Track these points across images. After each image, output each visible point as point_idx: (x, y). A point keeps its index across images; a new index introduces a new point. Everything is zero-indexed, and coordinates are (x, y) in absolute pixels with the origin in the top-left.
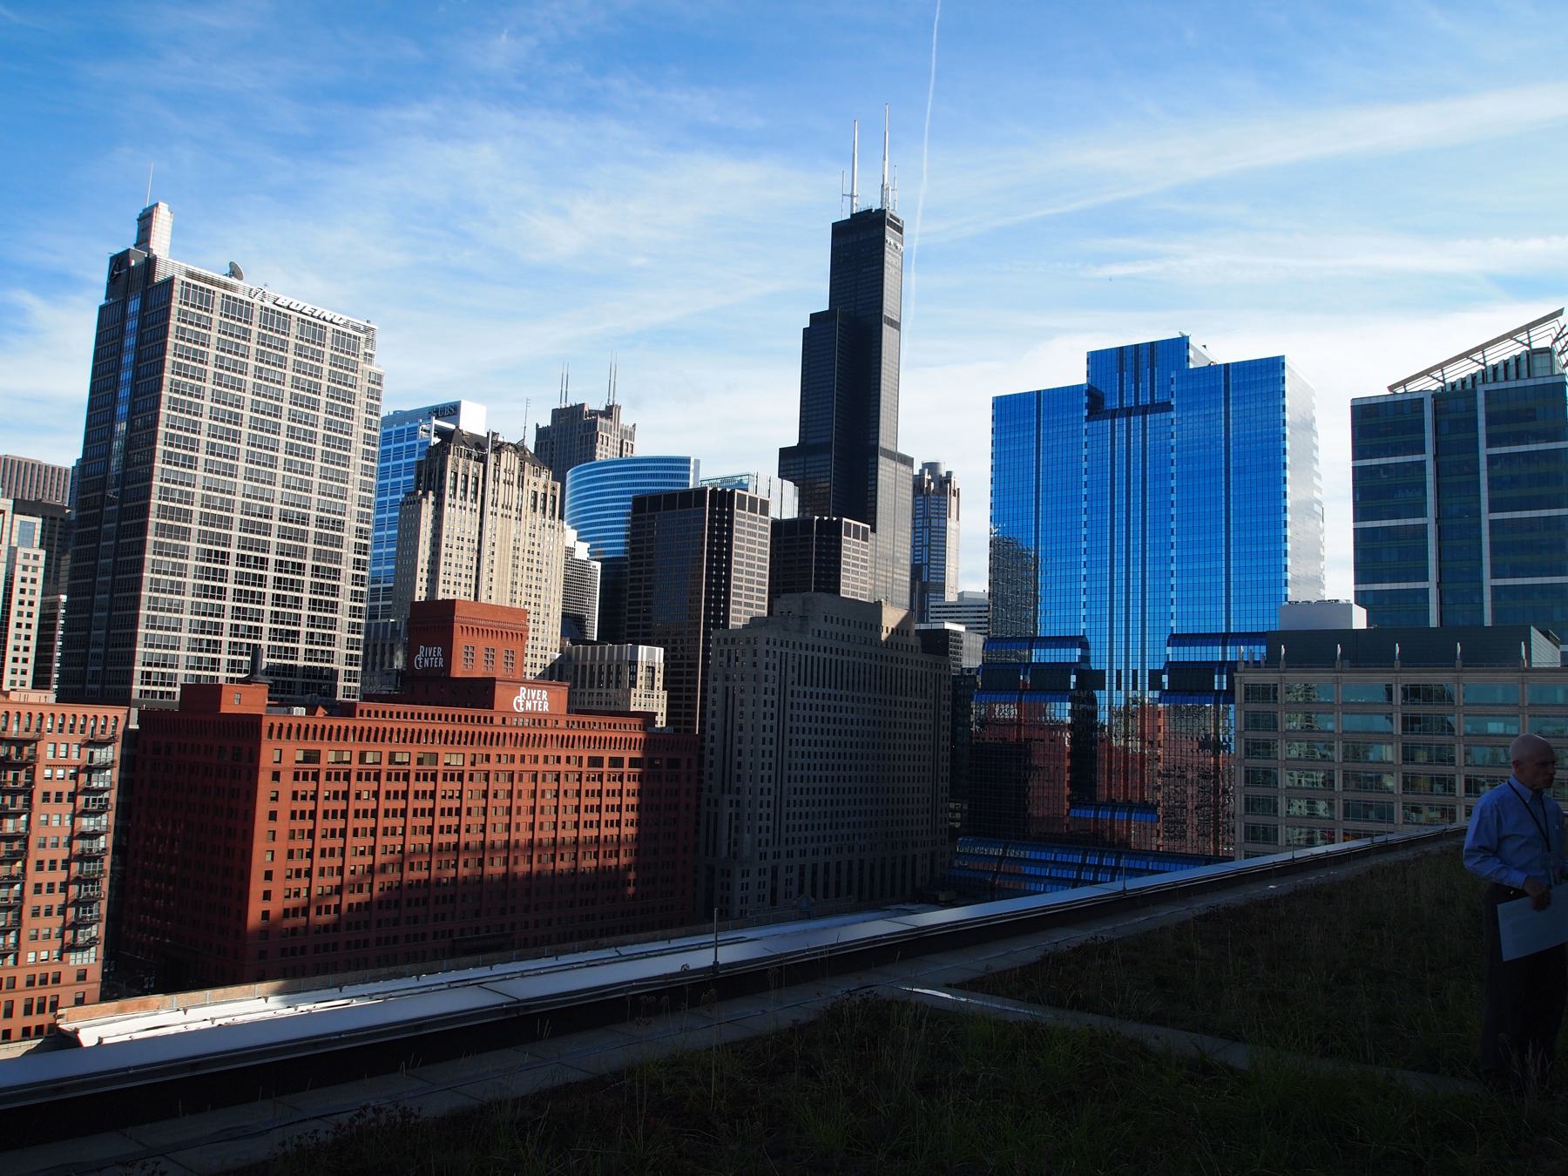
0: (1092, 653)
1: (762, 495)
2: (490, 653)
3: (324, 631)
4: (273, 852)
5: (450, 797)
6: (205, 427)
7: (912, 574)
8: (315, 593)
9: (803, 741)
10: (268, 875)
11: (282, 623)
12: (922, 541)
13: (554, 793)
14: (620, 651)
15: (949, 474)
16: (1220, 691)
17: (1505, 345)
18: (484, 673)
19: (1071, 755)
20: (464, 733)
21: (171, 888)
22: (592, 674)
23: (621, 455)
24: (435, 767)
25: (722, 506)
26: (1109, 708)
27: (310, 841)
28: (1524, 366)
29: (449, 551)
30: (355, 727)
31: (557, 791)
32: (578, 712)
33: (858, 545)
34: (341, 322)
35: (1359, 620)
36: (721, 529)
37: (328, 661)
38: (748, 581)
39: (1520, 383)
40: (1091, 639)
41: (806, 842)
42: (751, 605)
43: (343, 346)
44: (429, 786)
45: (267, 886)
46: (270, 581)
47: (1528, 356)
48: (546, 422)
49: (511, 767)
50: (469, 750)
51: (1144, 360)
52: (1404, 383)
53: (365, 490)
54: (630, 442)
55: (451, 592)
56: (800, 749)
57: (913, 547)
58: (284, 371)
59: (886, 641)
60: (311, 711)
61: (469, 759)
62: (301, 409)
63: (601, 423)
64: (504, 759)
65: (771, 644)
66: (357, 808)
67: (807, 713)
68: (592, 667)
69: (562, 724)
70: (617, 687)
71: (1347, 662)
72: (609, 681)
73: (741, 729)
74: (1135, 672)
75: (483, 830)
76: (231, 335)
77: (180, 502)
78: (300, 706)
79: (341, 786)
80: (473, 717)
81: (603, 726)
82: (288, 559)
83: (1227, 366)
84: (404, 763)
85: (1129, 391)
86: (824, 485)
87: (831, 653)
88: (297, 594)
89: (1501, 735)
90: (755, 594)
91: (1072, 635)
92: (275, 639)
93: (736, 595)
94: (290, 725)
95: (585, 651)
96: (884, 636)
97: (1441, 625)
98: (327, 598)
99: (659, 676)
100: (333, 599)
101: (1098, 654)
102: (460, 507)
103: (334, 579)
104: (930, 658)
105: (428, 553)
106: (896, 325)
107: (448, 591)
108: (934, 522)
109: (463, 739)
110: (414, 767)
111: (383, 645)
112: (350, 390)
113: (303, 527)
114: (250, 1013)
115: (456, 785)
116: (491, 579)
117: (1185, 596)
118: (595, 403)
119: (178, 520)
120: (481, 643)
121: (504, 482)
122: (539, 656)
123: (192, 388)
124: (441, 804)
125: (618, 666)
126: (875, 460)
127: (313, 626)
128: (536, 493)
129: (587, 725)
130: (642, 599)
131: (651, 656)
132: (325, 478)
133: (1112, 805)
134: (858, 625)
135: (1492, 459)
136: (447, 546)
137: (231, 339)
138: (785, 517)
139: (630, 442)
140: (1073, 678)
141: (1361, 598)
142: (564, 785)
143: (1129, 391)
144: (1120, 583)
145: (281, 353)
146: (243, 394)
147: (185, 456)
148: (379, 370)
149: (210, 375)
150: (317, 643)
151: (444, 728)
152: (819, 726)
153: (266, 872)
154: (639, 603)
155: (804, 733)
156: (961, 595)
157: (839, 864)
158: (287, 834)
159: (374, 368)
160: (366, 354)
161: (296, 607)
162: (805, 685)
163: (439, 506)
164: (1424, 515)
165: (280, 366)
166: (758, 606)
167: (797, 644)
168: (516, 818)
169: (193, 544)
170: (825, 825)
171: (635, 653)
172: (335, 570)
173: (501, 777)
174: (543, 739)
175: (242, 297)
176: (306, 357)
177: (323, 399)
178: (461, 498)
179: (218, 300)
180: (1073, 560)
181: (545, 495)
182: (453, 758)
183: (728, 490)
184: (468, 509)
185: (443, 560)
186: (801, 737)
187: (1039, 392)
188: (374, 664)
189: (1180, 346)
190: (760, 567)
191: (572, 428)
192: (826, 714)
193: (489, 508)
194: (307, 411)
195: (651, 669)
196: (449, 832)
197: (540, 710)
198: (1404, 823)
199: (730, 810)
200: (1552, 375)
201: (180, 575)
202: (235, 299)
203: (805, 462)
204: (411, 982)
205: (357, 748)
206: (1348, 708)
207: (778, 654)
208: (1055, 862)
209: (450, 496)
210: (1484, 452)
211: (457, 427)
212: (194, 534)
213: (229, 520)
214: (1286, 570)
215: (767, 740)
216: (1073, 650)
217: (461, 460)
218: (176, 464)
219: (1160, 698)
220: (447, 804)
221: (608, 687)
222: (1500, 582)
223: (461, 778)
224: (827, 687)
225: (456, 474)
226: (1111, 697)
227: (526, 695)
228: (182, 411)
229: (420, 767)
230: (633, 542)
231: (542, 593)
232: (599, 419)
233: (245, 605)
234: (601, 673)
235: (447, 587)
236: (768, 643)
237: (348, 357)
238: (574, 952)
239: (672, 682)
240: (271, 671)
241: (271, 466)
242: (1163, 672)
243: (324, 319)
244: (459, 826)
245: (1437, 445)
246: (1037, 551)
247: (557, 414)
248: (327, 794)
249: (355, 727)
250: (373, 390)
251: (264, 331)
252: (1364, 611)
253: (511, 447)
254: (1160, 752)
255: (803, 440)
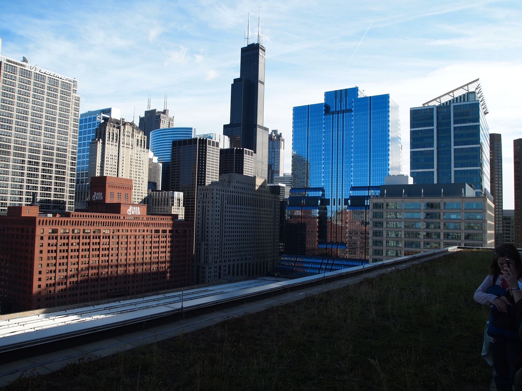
0: (326, 193)
1: (217, 140)
2: (119, 194)
3: (61, 187)
4: (41, 264)
5: (105, 244)
6: (15, 116)
7: (268, 167)
8: (57, 174)
9: (229, 223)
10: (40, 272)
11: (45, 185)
12: (272, 156)
13: (142, 242)
14: (168, 194)
15: (281, 134)
16: (367, 205)
17: (461, 90)
18: (117, 201)
19: (318, 227)
20: (110, 222)
21: (6, 278)
22: (159, 201)
23: (169, 127)
24: (100, 234)
25: (203, 144)
26: (331, 211)
27: (67, 260)
28: (466, 98)
29: (108, 159)
30: (70, 221)
31: (144, 242)
32: (152, 214)
33: (249, 157)
34: (64, 79)
35: (411, 181)
36: (202, 152)
37: (62, 198)
38: (212, 170)
39: (465, 103)
40: (325, 189)
41: (231, 257)
42: (213, 178)
43: (65, 87)
44: (98, 241)
45: (40, 276)
46: (40, 170)
47: (467, 94)
48: (143, 115)
49: (127, 234)
50: (112, 228)
51: (344, 95)
52: (427, 103)
53: (74, 138)
54: (172, 122)
55: (109, 174)
56: (228, 226)
57: (269, 158)
58: (44, 96)
59: (258, 190)
60: (54, 215)
61: (112, 231)
62: (50, 109)
63: (162, 116)
64: (124, 231)
65: (218, 191)
66: (82, 248)
67: (231, 214)
68: (158, 199)
69: (145, 219)
70: (167, 206)
71: (406, 195)
72: (164, 204)
73: (208, 220)
74: (340, 199)
75: (118, 255)
76: (24, 83)
77: (21, 145)
78: (50, 214)
79: (66, 241)
80: (113, 217)
81: (159, 219)
82: (46, 162)
83: (370, 97)
84: (88, 233)
85: (338, 105)
86: (238, 137)
87: (239, 193)
88: (50, 175)
89: (455, 219)
90: (214, 174)
91: (319, 187)
92: (42, 190)
93: (208, 174)
94: (47, 220)
95: (156, 194)
96: (257, 188)
97: (438, 183)
98: (61, 176)
99: (182, 202)
100: (63, 176)
101: (327, 193)
102: (111, 144)
103: (64, 169)
104: (273, 195)
105: (100, 160)
106: (263, 83)
107: (108, 174)
108: (276, 150)
109: (110, 224)
110: (92, 234)
111: (85, 192)
112: (68, 102)
113: (52, 151)
114: (32, 321)
115: (108, 240)
116: (123, 169)
117: (356, 174)
118: (160, 109)
119: (6, 148)
120: (116, 191)
121: (127, 136)
122: (140, 196)
123: (9, 102)
124: (102, 247)
125: (167, 199)
126: (255, 129)
127: (56, 186)
128: (138, 140)
129: (154, 219)
130: (176, 176)
131: (179, 195)
132: (60, 134)
133: (332, 243)
134: (248, 184)
135: (455, 128)
136: (107, 158)
137: (23, 84)
138: (225, 148)
139: (172, 122)
140: (319, 202)
141: (412, 174)
142: (146, 239)
143: (338, 105)
144: (335, 170)
145: (42, 89)
146: (29, 104)
147: (7, 126)
148: (79, 96)
149: (16, 97)
150: (58, 192)
151: (103, 221)
152: (235, 218)
153: (39, 271)
154: (175, 177)
155: (229, 221)
156: (284, 174)
157: (242, 264)
158: (46, 258)
159: (77, 95)
160: (74, 90)
161: (50, 179)
162: (230, 204)
163: (104, 144)
164: (433, 147)
165: (42, 94)
166: (215, 178)
167: (227, 191)
168: (129, 251)
169: (12, 157)
170: (237, 251)
171: (173, 194)
172: (64, 166)
173: (124, 237)
174: (138, 224)
175: (27, 69)
176: (51, 91)
177: (58, 106)
178: (112, 141)
179: (18, 70)
180: (320, 162)
181: (141, 140)
182: (106, 231)
183: (205, 139)
184: (114, 145)
185: (105, 163)
186: (228, 222)
187: (308, 106)
188: (79, 199)
189: (355, 90)
190: (216, 165)
191: (152, 117)
192: (237, 214)
193: (121, 145)
194: (52, 110)
195: (179, 200)
196: (105, 256)
197: (137, 214)
198: (424, 248)
199: (204, 247)
200: (475, 100)
201: (7, 168)
202: (25, 70)
203: (232, 130)
204: (91, 308)
205: (71, 228)
206: (407, 211)
207: (220, 194)
208: (313, 262)
209: (108, 141)
210: (453, 126)
211: (110, 117)
212: (12, 154)
213: (25, 149)
214: (389, 165)
215: (217, 223)
216: (319, 192)
217: (111, 128)
218: (4, 129)
219: (348, 208)
220: (104, 247)
221: (164, 206)
222: (457, 169)
223: (109, 238)
224: (237, 205)
225: (110, 133)
226: (332, 208)
227: (132, 209)
228: (6, 110)
229: (94, 234)
230: (172, 156)
231: (141, 174)
232: (161, 115)
233: (31, 178)
234: (161, 201)
235: (107, 172)
236: (217, 191)
237: (67, 91)
238: (149, 296)
239: (186, 204)
240: (41, 201)
241: (40, 129)
242: (349, 199)
243: (58, 77)
244: (109, 254)
245: (438, 123)
246: (307, 159)
247: (147, 113)
248: (61, 244)
249: (70, 221)
250: (77, 103)
251: (36, 82)
252: (412, 178)
253: (129, 124)
254: (347, 225)
255: (231, 122)
